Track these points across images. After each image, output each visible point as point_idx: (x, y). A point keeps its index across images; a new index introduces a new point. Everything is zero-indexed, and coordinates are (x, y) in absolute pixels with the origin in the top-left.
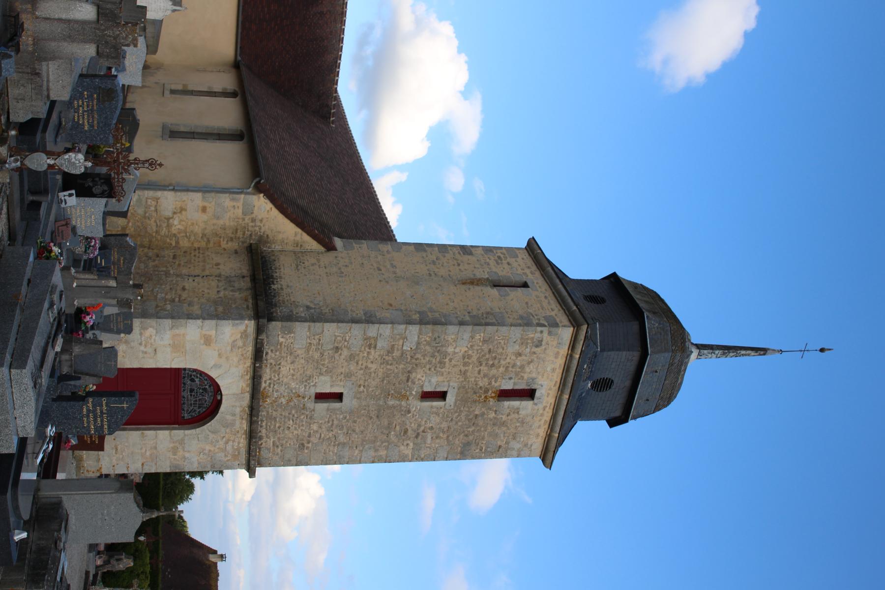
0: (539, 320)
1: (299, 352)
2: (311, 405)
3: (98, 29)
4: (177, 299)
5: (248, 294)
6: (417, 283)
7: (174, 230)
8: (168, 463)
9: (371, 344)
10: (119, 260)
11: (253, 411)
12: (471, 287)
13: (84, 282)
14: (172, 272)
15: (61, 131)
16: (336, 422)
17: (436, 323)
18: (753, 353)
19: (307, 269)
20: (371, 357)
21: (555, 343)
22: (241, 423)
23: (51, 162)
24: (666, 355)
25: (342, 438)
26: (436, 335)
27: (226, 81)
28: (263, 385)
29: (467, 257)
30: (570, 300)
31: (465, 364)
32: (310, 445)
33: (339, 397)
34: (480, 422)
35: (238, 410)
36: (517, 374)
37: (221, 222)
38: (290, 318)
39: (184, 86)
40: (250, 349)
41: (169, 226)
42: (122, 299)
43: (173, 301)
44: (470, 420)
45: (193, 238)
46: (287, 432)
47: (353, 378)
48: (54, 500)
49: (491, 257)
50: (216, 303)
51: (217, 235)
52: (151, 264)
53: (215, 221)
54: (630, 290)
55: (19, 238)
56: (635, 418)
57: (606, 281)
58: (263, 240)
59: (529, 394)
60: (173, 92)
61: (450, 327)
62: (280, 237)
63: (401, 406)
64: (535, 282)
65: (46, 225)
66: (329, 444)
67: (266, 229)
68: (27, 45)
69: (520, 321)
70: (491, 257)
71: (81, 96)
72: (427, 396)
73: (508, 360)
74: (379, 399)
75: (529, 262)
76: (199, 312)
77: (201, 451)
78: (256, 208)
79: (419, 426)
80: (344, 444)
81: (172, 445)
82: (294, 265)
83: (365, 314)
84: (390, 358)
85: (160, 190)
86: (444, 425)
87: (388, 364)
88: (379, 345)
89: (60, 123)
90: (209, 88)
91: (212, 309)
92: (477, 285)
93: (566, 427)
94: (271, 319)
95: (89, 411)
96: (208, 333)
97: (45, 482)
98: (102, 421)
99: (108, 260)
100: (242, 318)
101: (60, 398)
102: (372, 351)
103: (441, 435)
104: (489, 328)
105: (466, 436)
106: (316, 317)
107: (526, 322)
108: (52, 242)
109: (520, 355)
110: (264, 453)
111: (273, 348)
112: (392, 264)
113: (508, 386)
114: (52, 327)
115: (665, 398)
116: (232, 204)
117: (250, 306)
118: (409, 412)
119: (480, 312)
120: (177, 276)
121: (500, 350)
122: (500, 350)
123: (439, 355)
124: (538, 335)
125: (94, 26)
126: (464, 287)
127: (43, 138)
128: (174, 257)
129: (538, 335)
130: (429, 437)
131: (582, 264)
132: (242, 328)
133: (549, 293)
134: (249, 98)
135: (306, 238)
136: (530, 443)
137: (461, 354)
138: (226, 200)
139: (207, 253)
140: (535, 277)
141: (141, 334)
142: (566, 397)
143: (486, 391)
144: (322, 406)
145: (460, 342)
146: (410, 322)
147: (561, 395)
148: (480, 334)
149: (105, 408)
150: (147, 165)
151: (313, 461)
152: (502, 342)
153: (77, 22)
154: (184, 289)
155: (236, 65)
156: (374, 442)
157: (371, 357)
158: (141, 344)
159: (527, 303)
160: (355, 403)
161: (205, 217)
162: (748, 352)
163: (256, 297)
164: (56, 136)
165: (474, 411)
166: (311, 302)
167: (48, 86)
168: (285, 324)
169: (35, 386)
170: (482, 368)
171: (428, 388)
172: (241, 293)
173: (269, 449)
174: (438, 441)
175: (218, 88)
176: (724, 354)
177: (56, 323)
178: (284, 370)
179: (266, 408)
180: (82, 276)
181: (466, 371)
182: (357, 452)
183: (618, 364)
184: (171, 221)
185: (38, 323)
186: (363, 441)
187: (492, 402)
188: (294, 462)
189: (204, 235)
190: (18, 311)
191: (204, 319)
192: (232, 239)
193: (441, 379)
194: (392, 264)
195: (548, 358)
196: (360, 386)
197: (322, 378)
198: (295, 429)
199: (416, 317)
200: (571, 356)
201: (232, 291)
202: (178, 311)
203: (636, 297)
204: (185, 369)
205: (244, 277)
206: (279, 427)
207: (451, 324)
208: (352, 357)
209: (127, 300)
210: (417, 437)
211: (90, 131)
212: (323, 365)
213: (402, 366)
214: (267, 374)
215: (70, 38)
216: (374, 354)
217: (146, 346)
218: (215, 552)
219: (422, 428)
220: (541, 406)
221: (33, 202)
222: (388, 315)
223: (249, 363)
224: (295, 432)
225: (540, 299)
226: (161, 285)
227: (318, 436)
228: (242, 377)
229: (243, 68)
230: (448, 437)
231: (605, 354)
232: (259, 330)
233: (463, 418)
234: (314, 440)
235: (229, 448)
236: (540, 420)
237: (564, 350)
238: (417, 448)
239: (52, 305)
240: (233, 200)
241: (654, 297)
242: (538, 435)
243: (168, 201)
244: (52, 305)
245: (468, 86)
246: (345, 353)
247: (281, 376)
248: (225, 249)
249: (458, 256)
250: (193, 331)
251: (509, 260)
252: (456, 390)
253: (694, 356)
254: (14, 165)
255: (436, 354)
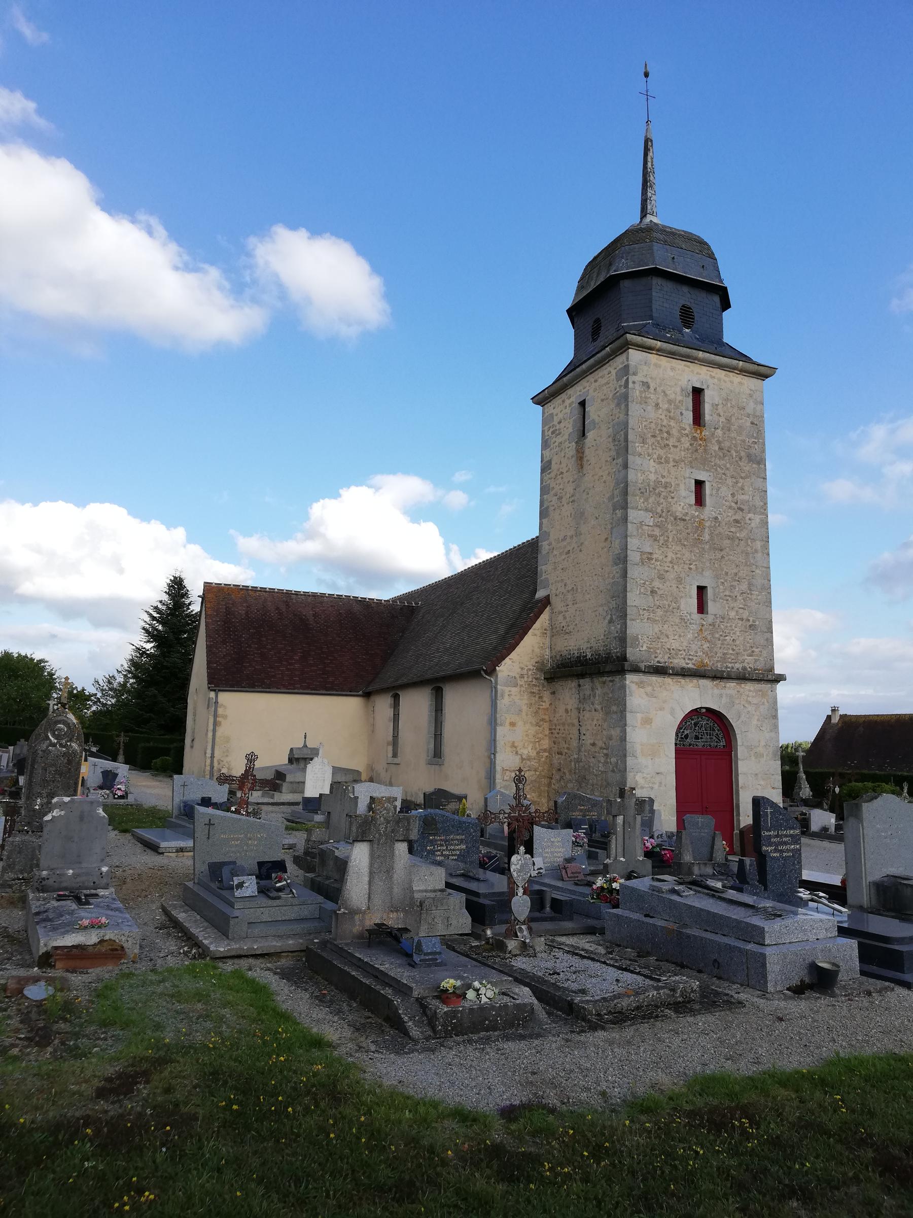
0: (620, 386)
1: (657, 630)
2: (710, 618)
3: (379, 840)
4: (605, 751)
5: (598, 682)
6: (582, 514)
7: (533, 754)
8: (772, 762)
9: (648, 558)
10: (581, 810)
11: (717, 676)
12: (585, 459)
13: (620, 850)
14: (576, 756)
15: (471, 874)
16: (727, 593)
17: (625, 493)
18: (650, 154)
19: (569, 623)
20: (661, 558)
21: (645, 368)
22: (729, 688)
23: (520, 891)
24: (655, 248)
25: (744, 587)
26: (638, 492)
27: (383, 704)
28: (690, 666)
29: (554, 466)
30: (599, 355)
31: (667, 462)
32: (751, 619)
33: (701, 590)
34: (727, 444)
35: (716, 691)
36: (677, 407)
37: (525, 708)
38: (622, 639)
39: (388, 744)
40: (655, 679)
41: (529, 759)
42: (636, 810)
43: (606, 755)
44: (724, 456)
45: (540, 735)
46: (738, 642)
47: (683, 575)
48: (873, 891)
49: (553, 441)
50: (608, 713)
51: (536, 712)
52: (568, 776)
53: (524, 714)
54: (585, 293)
55: (590, 922)
56: (721, 281)
57: (576, 320)
58: (540, 667)
59: (697, 393)
60: (395, 755)
61: (630, 478)
62: (537, 650)
63: (710, 527)
64: (578, 393)
65: (571, 892)
66: (750, 599)
67: (529, 664)
68: (398, 919)
69: (623, 406)
70: (553, 441)
71: (432, 852)
72: (700, 500)
73: (663, 417)
74: (703, 549)
75: (558, 401)
76: (618, 730)
77: (759, 728)
78: (511, 674)
79: (730, 507)
80: (750, 584)
81: (753, 758)
82: (566, 636)
83: (617, 564)
84: (662, 538)
85: (495, 767)
86: (730, 481)
87: (667, 541)
88: (649, 550)
89: (463, 875)
90: (390, 721)
91: (615, 716)
92: (583, 453)
93: (732, 354)
94: (625, 659)
95: (776, 850)
96: (639, 722)
97: (850, 899)
98: (786, 836)
99: (582, 822)
100: (623, 687)
101: (763, 880)
102: (654, 556)
103: (739, 485)
104: (630, 437)
105: (741, 459)
106: (621, 613)
107: (623, 400)
108: (591, 886)
109: (657, 405)
110: (760, 665)
111: (653, 656)
112: (562, 540)
113: (689, 416)
114: (699, 892)
115: (701, 248)
116: (506, 697)
117: (610, 678)
118: (716, 518)
119: (613, 448)
120: (580, 751)
121: (653, 425)
122: (653, 425)
123: (660, 488)
124: (637, 386)
125: (376, 846)
126: (585, 467)
127: (485, 896)
128: (560, 753)
129: (637, 386)
130: (743, 497)
131: (560, 345)
132: (633, 687)
133: (591, 378)
134: (396, 684)
135: (537, 625)
136: (748, 392)
137: (657, 466)
138: (503, 703)
139: (555, 721)
140: (574, 395)
141: (642, 788)
142: (701, 354)
143: (694, 439)
144: (711, 607)
145: (644, 468)
146: (625, 519)
147: (699, 360)
148: (636, 446)
149: (772, 833)
150: (521, 786)
151: (767, 616)
152: (644, 423)
153: (371, 865)
154: (594, 744)
155: (367, 695)
156: (747, 554)
157: (661, 558)
158: (652, 788)
159: (602, 400)
160: (708, 573)
161: (520, 724)
162: (649, 159)
163: (601, 673)
164: (478, 880)
165: (715, 451)
166: (604, 618)
167: (431, 891)
168: (628, 645)
169: (780, 916)
170: (671, 444)
171: (692, 499)
172: (598, 688)
173: (756, 661)
174: (746, 488)
175: (390, 712)
176: (651, 186)
177: (694, 887)
178: (675, 645)
179: (713, 663)
180: (613, 852)
181: (674, 461)
182: (757, 571)
183: (666, 300)
184: (524, 757)
185: (701, 909)
186: (746, 565)
187: (706, 433)
188: (767, 635)
189: (537, 725)
190: (688, 931)
191: (626, 725)
192: (540, 697)
193: (682, 487)
194: (562, 540)
195: (659, 375)
196: (690, 569)
197: (682, 607)
198: (734, 633)
199: (619, 513)
200: (658, 350)
201: (594, 697)
202: (618, 751)
203: (593, 286)
204: (676, 744)
205: (579, 686)
206: (733, 650)
207: (626, 477)
208: (661, 577)
209: (636, 804)
210: (742, 510)
211: (466, 843)
212: (669, 606)
213: (670, 527)
214: (679, 662)
215: (389, 871)
216: (658, 554)
217: (654, 783)
218: (829, 717)
219: (733, 504)
220: (711, 381)
221: (552, 907)
222: (617, 542)
223: (668, 680)
224: (738, 633)
225: (597, 388)
226: (589, 766)
227: (741, 611)
228: (682, 687)
229: (370, 689)
230: (742, 478)
231: (654, 315)
232: (636, 670)
233: (723, 462)
234: (745, 615)
235: (755, 701)
236: (725, 382)
237: (653, 358)
238: (753, 509)
239: (673, 891)
240: (502, 696)
241: (593, 266)
242: (740, 383)
243: (506, 761)
244: (673, 891)
245: (370, 486)
246: (657, 584)
247: (681, 648)
248: (551, 704)
249: (553, 475)
250: (638, 736)
251: (555, 422)
252: (693, 470)
253: (655, 220)
254: (525, 933)
255: (657, 491)
